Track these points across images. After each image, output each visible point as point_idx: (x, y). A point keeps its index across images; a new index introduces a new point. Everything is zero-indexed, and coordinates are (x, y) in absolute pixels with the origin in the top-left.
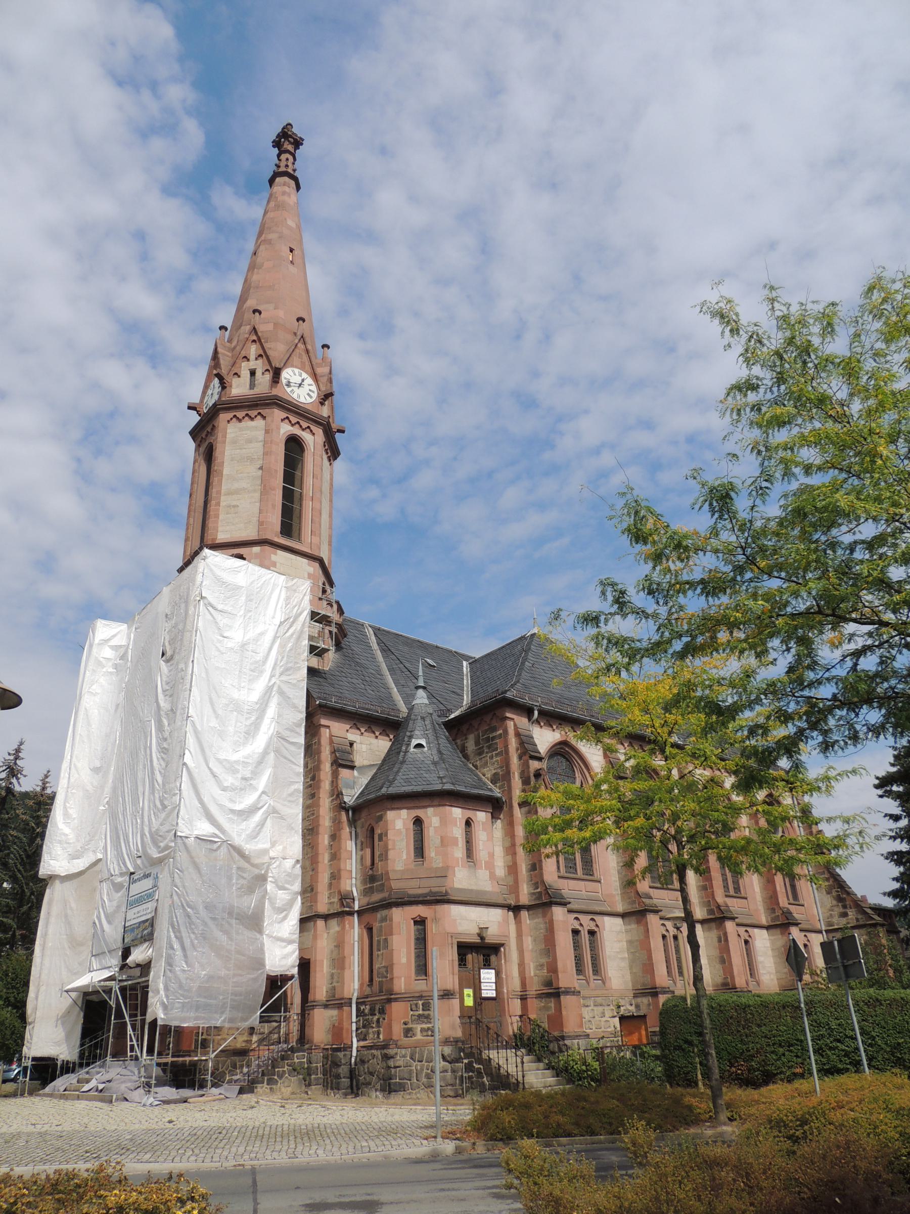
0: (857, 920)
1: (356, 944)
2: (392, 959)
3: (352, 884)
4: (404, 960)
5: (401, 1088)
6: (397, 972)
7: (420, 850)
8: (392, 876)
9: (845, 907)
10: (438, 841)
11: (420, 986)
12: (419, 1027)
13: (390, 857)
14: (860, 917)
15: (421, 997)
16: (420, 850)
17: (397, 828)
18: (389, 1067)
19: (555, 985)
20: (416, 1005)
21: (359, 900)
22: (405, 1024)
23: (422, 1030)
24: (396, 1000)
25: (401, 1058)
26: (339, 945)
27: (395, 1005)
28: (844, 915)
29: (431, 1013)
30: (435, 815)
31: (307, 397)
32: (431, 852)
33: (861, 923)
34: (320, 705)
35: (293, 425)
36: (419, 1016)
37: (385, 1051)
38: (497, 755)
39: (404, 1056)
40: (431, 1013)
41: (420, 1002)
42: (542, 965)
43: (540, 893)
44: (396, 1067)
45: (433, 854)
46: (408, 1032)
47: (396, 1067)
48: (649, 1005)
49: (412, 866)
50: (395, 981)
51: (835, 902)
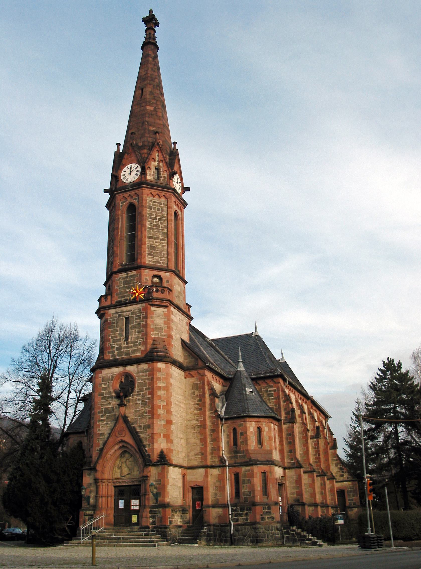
0: (348, 478)
1: (228, 480)
2: (254, 488)
3: (224, 453)
4: (259, 489)
5: (262, 541)
6: (170, 488)
7: (260, 442)
8: (250, 452)
9: (343, 472)
10: (268, 438)
11: (265, 499)
12: (266, 517)
13: (248, 443)
14: (349, 477)
15: (267, 504)
16: (260, 442)
17: (251, 430)
18: (257, 533)
19: (301, 501)
20: (266, 508)
21: (228, 461)
22: (261, 515)
23: (268, 518)
24: (257, 505)
25: (261, 529)
26: (221, 479)
27: (257, 507)
28: (342, 476)
29: (271, 511)
30: (266, 426)
31: (137, 170)
32: (265, 443)
33: (349, 479)
34: (208, 366)
35: (154, 196)
36: (267, 512)
37: (254, 526)
38: (272, 399)
39: (262, 529)
40: (271, 511)
41: (267, 507)
42: (293, 493)
43: (294, 463)
44: (259, 533)
45: (266, 444)
46: (263, 519)
47: (259, 533)
48: (313, 510)
49: (257, 448)
50: (256, 498)
51: (339, 470)
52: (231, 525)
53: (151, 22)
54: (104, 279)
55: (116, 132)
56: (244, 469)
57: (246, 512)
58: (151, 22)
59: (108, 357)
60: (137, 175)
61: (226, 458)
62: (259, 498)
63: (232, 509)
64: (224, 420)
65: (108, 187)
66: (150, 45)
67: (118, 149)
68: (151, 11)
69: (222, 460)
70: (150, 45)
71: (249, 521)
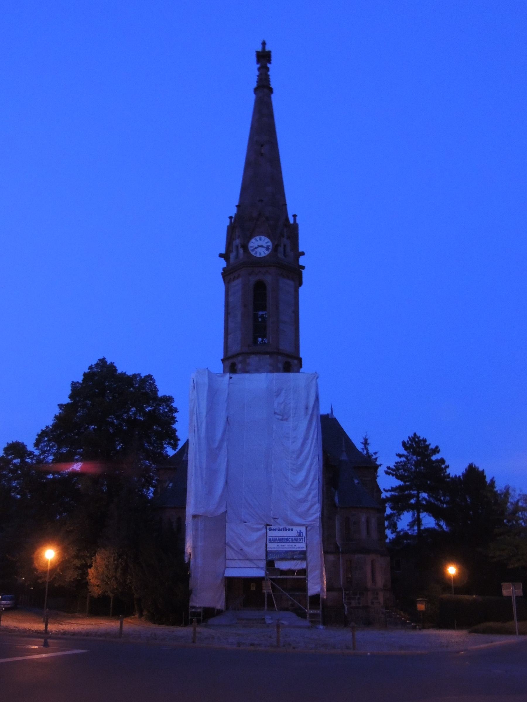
46: (372, 603)
52: (344, 608)
53: (264, 57)
54: (274, 98)
55: (226, 198)
56: (356, 556)
57: (358, 596)
58: (264, 57)
59: (230, 354)
60: (260, 240)
61: (339, 545)
62: (369, 584)
63: (345, 593)
64: (339, 509)
65: (223, 251)
66: (264, 88)
67: (231, 221)
68: (264, 44)
69: (337, 547)
70: (264, 88)
71: (361, 605)
